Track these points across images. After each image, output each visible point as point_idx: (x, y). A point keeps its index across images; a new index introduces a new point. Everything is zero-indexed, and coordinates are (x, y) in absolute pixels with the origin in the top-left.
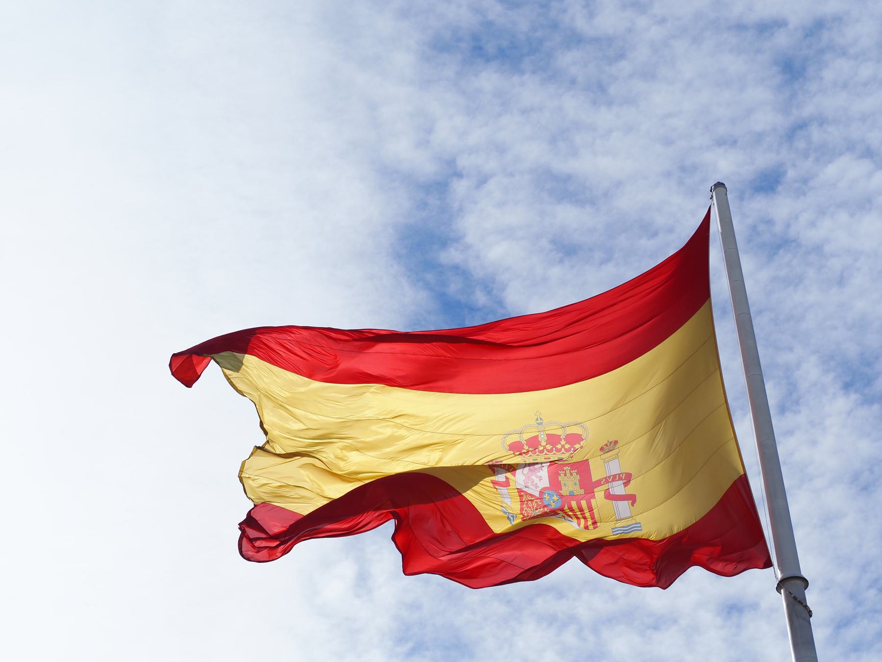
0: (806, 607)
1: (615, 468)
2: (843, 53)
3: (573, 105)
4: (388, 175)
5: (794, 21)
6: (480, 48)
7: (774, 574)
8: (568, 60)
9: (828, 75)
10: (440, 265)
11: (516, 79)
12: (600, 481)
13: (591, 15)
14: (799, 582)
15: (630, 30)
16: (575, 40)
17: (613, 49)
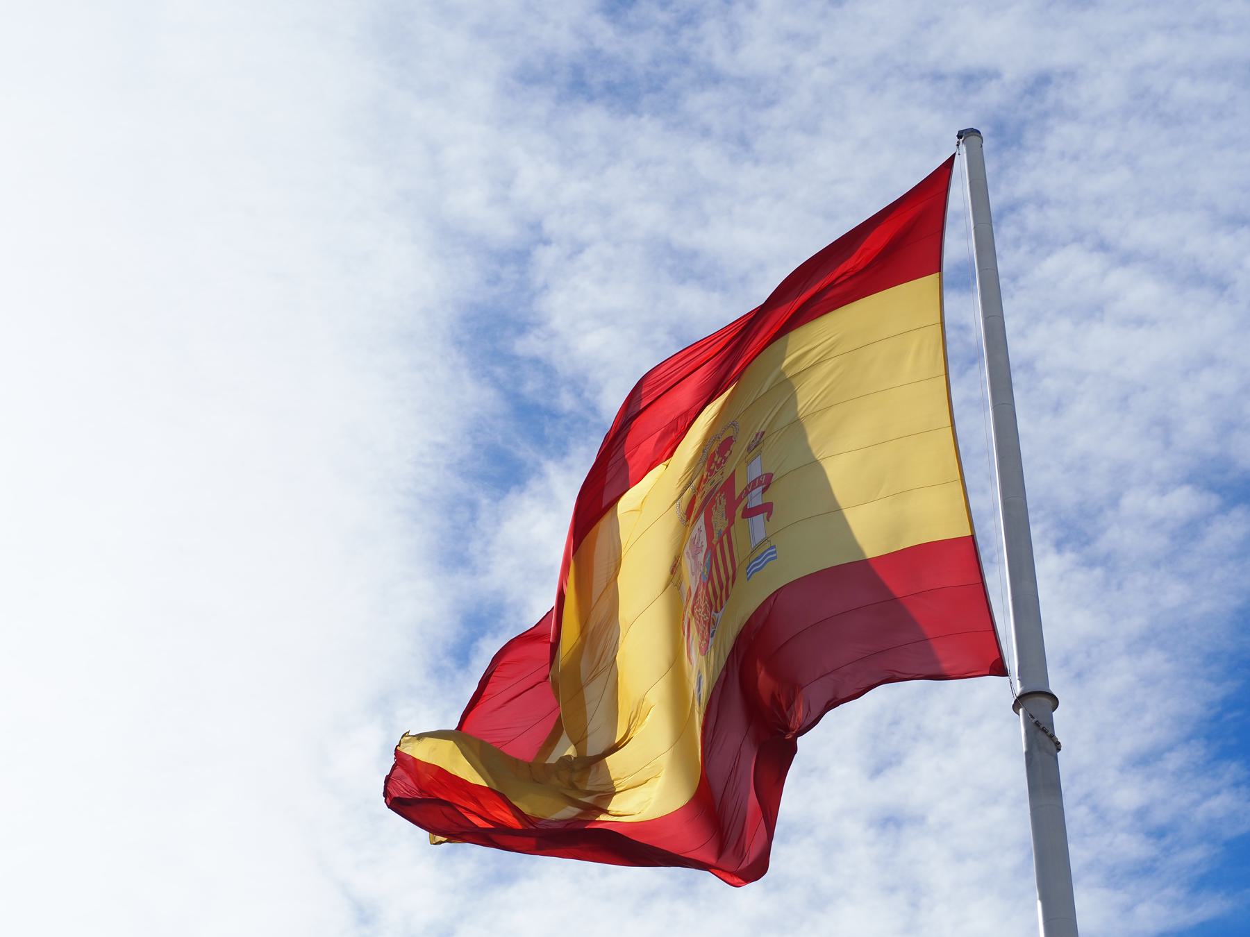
0: (1052, 736)
2: (1073, 116)
4: (450, 237)
5: (1009, 75)
6: (583, 84)
8: (699, 102)
9: (1053, 143)
10: (515, 357)
11: (631, 119)
13: (734, 48)
14: (1045, 700)
15: (787, 69)
16: (711, 78)
17: (760, 93)
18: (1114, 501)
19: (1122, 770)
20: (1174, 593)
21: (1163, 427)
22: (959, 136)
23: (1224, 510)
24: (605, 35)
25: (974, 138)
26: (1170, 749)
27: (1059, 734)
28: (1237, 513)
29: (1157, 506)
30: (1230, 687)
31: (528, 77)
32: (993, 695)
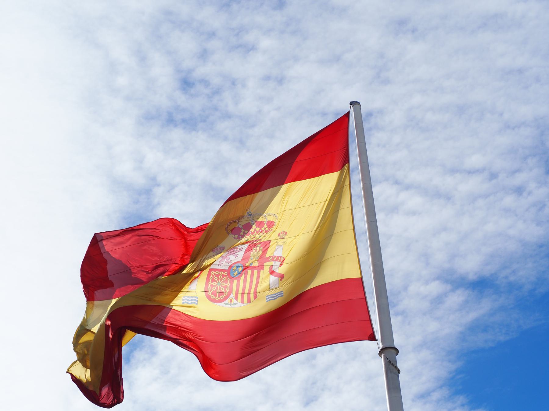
0: (396, 367)
1: (279, 253)
3: (226, 148)
4: (118, 184)
7: (374, 347)
8: (223, 126)
11: (194, 133)
12: (269, 258)
14: (393, 351)
15: (260, 111)
16: (227, 116)
18: (406, 288)
19: (413, 400)
20: (433, 326)
21: (425, 257)
22: (351, 104)
23: (453, 290)
24: (182, 99)
25: (357, 106)
26: (434, 391)
27: (399, 366)
28: (459, 291)
29: (424, 289)
30: (459, 364)
31: (149, 117)
32: (370, 348)
